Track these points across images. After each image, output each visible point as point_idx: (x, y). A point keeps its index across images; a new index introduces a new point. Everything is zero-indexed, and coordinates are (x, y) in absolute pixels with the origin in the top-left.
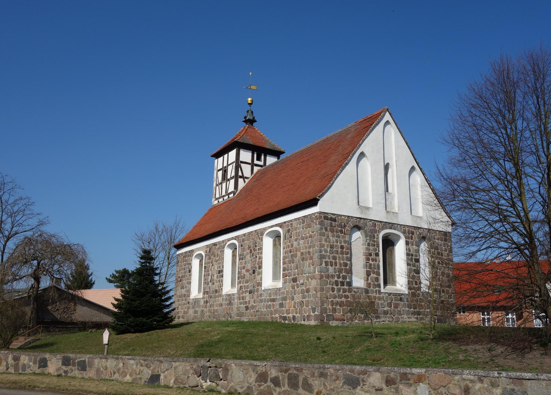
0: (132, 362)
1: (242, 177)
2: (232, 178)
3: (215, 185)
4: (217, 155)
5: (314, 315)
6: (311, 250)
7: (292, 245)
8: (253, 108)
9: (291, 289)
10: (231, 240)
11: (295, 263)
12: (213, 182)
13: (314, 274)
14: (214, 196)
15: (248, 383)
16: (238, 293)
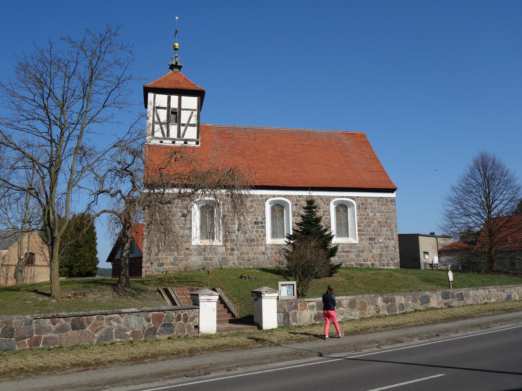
0: (494, 290)
3: (150, 121)
7: (368, 215)
10: (276, 197)
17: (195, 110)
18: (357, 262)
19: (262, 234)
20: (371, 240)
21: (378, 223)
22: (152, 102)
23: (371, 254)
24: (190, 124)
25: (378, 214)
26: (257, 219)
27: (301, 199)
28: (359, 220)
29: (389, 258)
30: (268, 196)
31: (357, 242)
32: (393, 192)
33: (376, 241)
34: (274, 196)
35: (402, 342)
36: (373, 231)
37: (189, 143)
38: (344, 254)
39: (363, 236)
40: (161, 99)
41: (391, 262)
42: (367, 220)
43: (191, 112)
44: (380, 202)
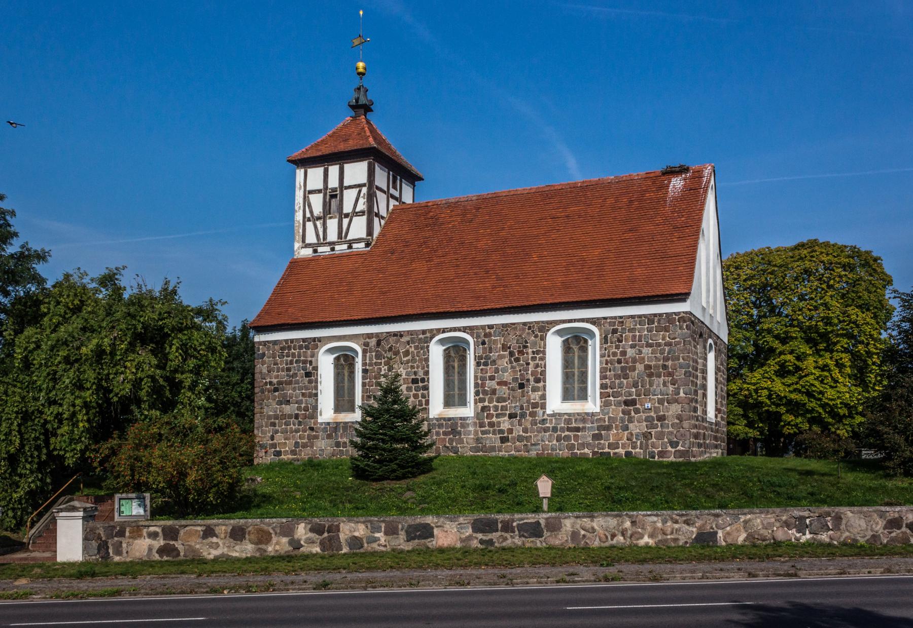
1: (377, 215)
2: (355, 214)
3: (299, 216)
4: (306, 162)
5: (676, 451)
6: (670, 363)
7: (624, 353)
8: (366, 82)
9: (621, 415)
10: (448, 332)
11: (630, 379)
12: (293, 212)
13: (677, 397)
14: (298, 237)
15: (872, 530)
16: (477, 415)
17: (364, 185)
18: (596, 450)
19: (424, 400)
20: (628, 406)
21: (646, 369)
22: (302, 184)
23: (626, 433)
24: (357, 213)
25: (647, 351)
26: (415, 373)
27: (492, 331)
28: (604, 365)
29: (666, 440)
30: (435, 332)
31: (598, 410)
32: (684, 300)
33: (638, 406)
34: (444, 331)
35: (728, 621)
36: (635, 385)
37: (355, 246)
38: (570, 433)
39: (611, 398)
40: (315, 176)
41: (669, 449)
42: (623, 364)
43: (358, 189)
44: (653, 323)
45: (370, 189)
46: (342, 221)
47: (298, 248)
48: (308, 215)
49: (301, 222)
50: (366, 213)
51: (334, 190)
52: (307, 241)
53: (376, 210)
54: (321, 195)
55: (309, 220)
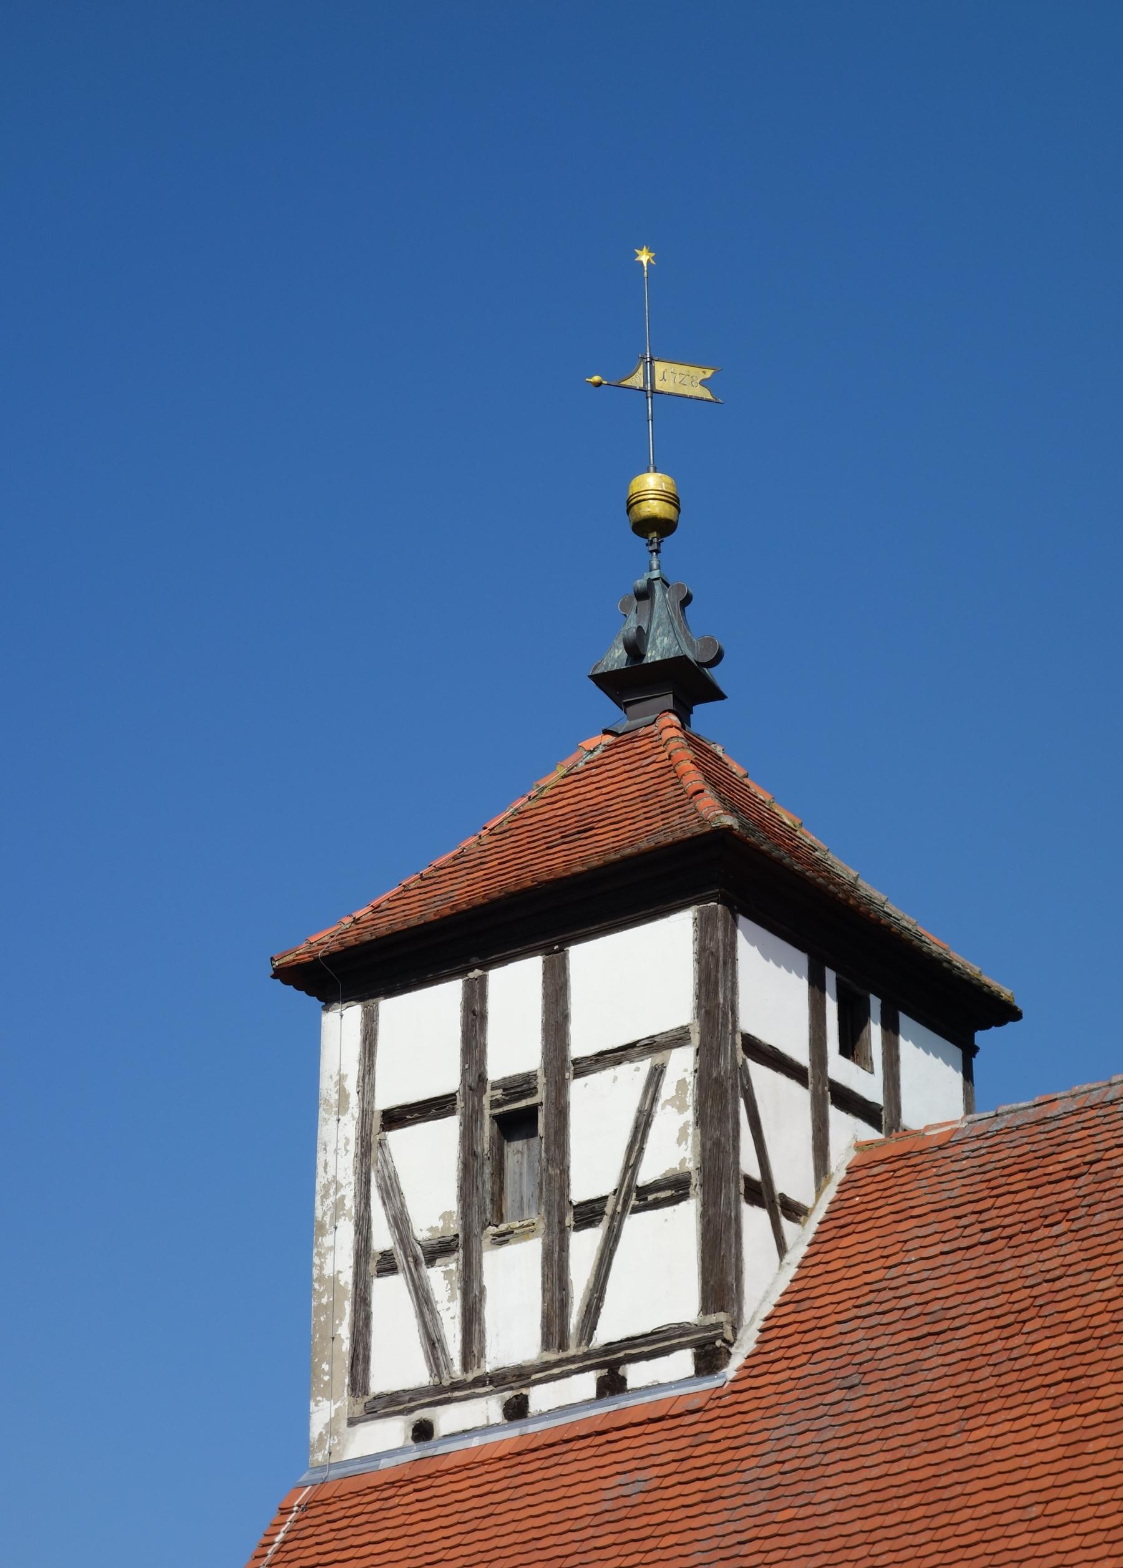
17: (679, 1038)
22: (352, 1085)
37: (637, 1374)
45: (707, 1056)
46: (564, 1248)
47: (331, 1428)
48: (383, 1239)
49: (347, 1278)
50: (695, 1190)
51: (520, 1086)
52: (381, 1381)
53: (749, 1165)
54: (449, 1128)
55: (387, 1266)
